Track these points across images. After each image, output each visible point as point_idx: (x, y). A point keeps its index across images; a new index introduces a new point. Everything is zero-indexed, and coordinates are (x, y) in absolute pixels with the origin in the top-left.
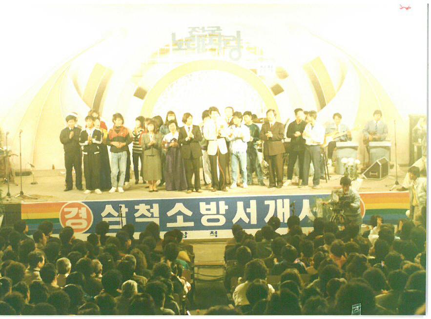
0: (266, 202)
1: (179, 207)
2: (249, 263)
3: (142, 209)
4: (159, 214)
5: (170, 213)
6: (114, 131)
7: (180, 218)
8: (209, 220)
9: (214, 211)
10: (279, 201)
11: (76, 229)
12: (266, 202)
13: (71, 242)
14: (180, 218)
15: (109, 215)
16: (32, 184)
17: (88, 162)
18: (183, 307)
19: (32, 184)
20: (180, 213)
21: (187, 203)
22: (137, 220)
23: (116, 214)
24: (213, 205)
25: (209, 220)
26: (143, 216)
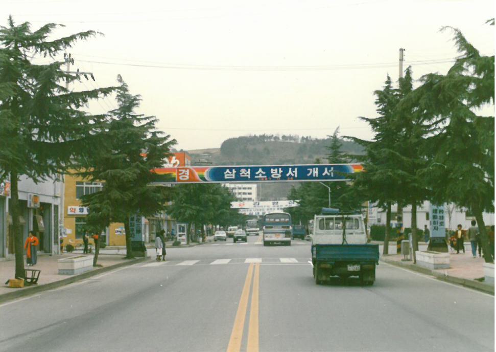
0: (308, 169)
1: (260, 170)
2: (5, 161)
3: (243, 171)
4: (17, 183)
5: (257, 173)
6: (453, 95)
7: (260, 175)
8: (275, 176)
9: (276, 172)
10: (314, 169)
11: (400, 76)
12: (308, 169)
13: (479, 74)
14: (260, 175)
15: (228, 173)
16: (83, 22)
17: (284, 137)
18: (162, 209)
19: (83, 22)
20: (260, 173)
21: (264, 169)
22: (241, 176)
23: (230, 173)
24: (276, 170)
25: (275, 176)
26: (243, 174)
